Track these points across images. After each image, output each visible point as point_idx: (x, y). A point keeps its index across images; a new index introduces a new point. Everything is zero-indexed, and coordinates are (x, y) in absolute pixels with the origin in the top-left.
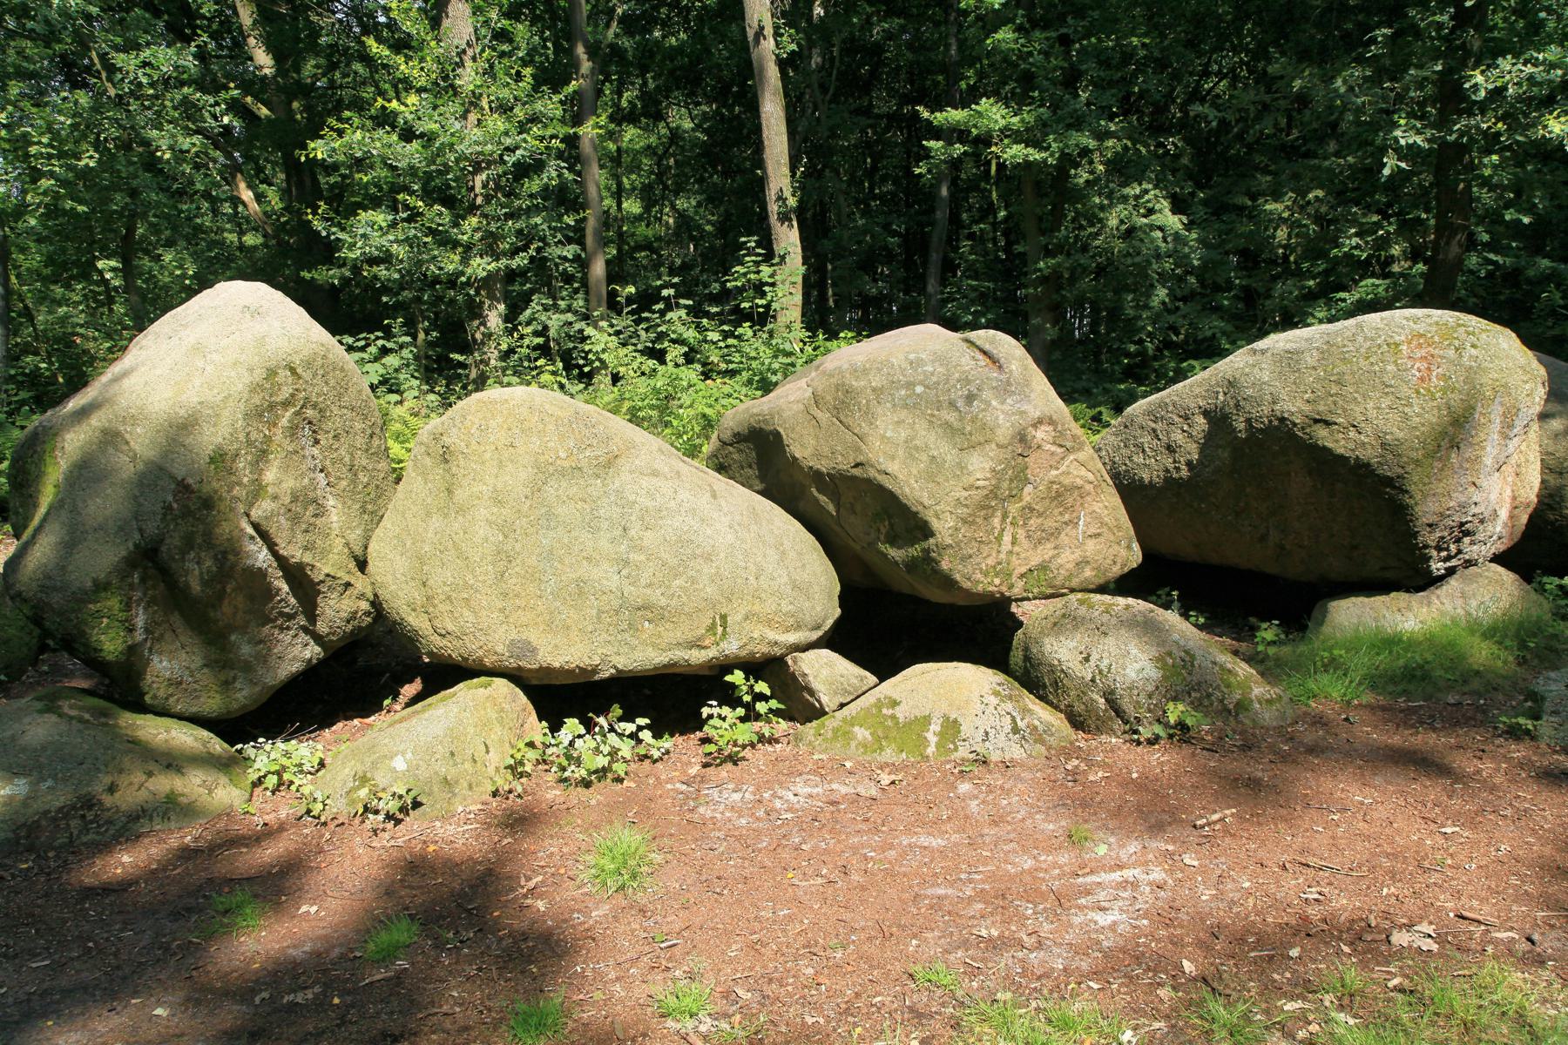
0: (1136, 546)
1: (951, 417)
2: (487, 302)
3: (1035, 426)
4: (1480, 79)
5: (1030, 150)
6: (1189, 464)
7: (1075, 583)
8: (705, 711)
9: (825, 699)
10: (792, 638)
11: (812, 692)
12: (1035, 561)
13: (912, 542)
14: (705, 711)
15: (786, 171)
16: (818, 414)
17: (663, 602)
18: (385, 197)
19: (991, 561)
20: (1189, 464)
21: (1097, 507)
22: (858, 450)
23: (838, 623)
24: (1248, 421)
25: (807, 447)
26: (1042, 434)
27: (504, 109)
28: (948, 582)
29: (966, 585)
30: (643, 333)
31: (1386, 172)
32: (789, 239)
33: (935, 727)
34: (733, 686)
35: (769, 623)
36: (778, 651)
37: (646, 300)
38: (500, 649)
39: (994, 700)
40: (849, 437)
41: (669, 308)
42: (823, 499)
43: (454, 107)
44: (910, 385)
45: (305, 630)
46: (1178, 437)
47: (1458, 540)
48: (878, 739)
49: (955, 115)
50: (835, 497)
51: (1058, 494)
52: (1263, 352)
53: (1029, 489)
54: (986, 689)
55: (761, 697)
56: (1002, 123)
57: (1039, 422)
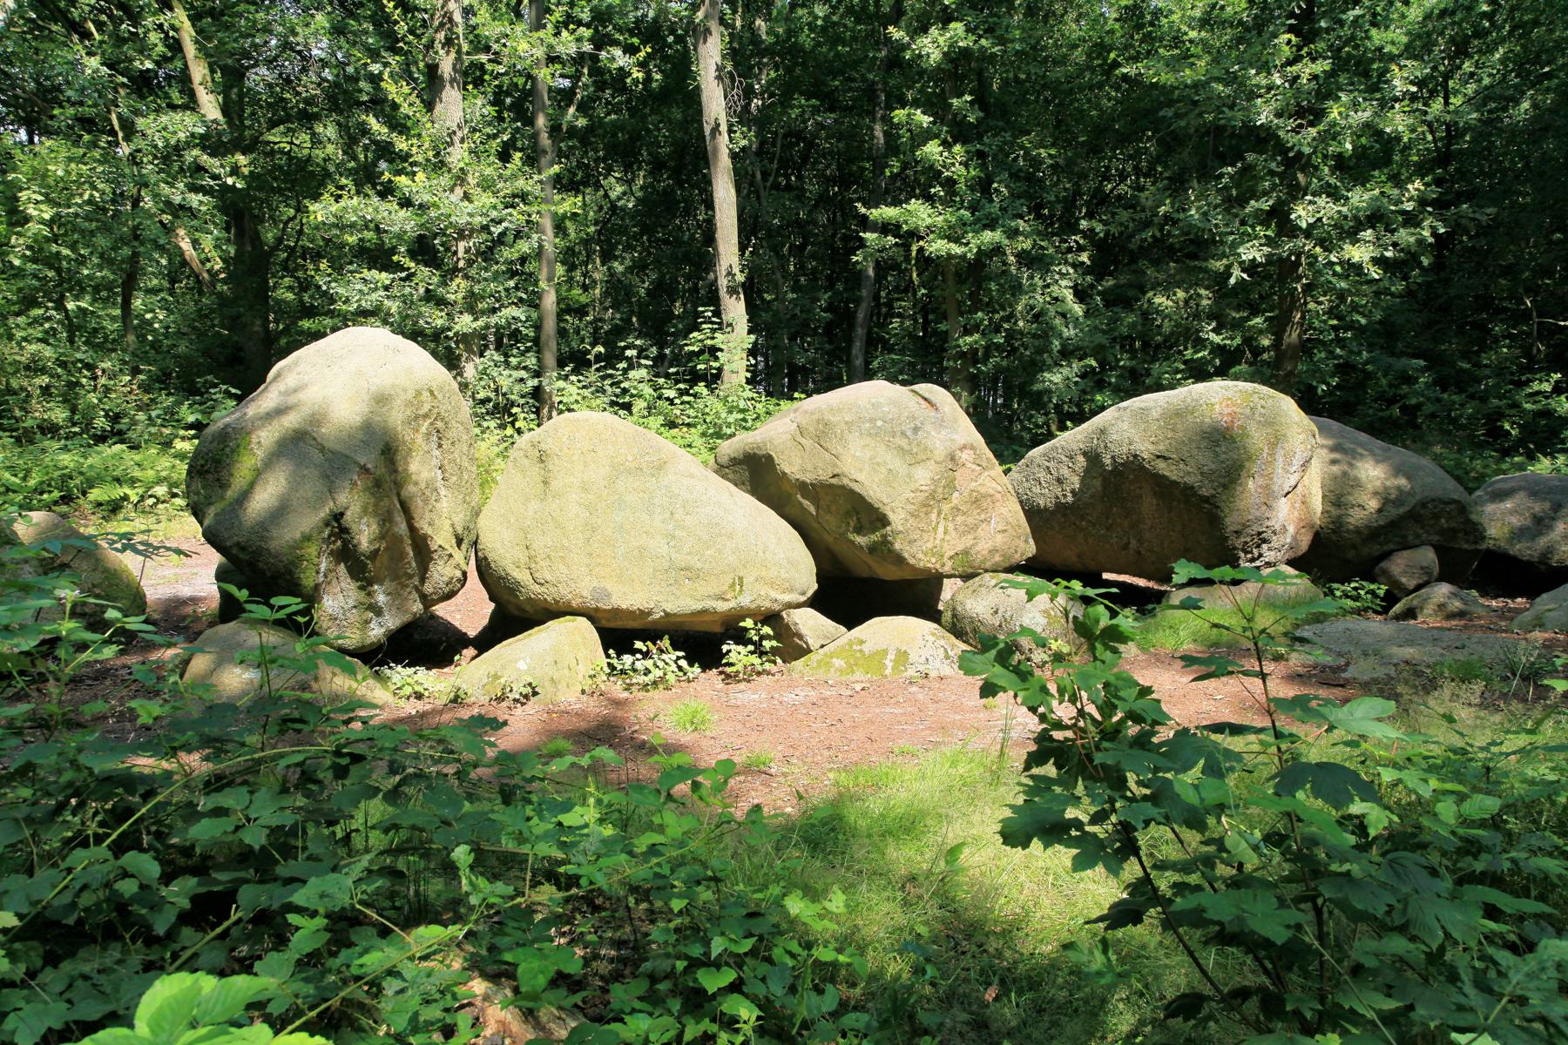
0: (1031, 541)
1: (903, 443)
2: (465, 355)
3: (961, 450)
4: (1303, 213)
5: (952, 245)
6: (1073, 491)
7: (988, 565)
8: (725, 648)
9: (810, 642)
10: (787, 598)
11: (801, 637)
12: (960, 548)
13: (877, 529)
14: (725, 648)
15: (735, 249)
16: (803, 441)
17: (699, 565)
18: (378, 256)
19: (930, 545)
20: (1073, 491)
21: (1004, 511)
22: (835, 465)
23: (816, 593)
24: (1113, 457)
25: (794, 465)
26: (965, 456)
27: (486, 185)
28: (899, 560)
29: (912, 561)
30: (607, 388)
31: (1232, 281)
32: (736, 310)
33: (891, 656)
34: (746, 630)
35: (772, 584)
36: (776, 607)
37: (611, 358)
38: (585, 593)
39: (932, 638)
40: (827, 455)
41: (631, 367)
42: (806, 503)
43: (445, 180)
44: (872, 420)
45: (416, 588)
46: (1065, 472)
47: (1258, 546)
48: (851, 666)
49: (887, 212)
50: (816, 501)
51: (977, 500)
52: (1125, 409)
53: (956, 494)
54: (927, 631)
55: (768, 637)
56: (929, 221)
57: (965, 447)
